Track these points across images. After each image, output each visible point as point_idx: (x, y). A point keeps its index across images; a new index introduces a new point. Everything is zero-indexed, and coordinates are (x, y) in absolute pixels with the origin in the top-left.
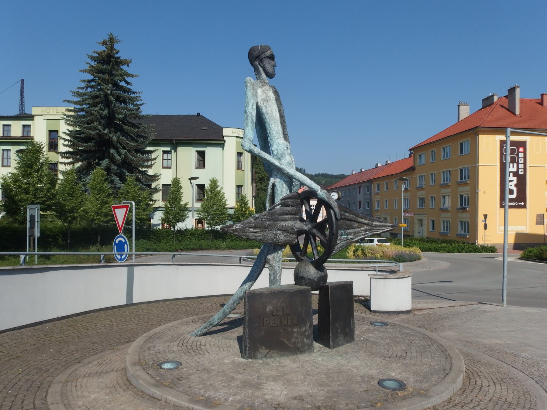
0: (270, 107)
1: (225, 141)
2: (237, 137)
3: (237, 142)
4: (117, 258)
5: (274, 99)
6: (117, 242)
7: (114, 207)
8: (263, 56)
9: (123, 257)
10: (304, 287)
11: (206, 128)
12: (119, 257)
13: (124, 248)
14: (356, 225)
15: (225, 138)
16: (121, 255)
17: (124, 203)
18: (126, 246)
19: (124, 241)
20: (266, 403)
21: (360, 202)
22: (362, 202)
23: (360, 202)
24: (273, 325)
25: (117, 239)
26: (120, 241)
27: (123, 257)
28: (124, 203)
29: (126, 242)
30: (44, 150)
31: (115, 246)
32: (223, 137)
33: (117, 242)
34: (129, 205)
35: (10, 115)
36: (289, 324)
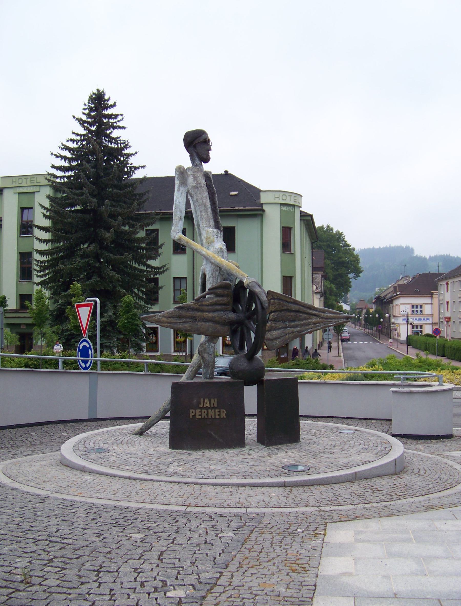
0: (201, 193)
1: (264, 211)
2: (282, 204)
3: (281, 211)
4: (82, 367)
5: (205, 186)
6: (81, 348)
7: (79, 306)
8: (196, 142)
9: (88, 365)
10: (237, 380)
11: (236, 193)
12: (83, 365)
13: (89, 355)
14: (304, 316)
15: (265, 207)
16: (85, 362)
17: (88, 301)
18: (90, 352)
19: (88, 346)
20: (205, 514)
21: (448, 303)
22: (450, 302)
23: (448, 303)
24: (200, 417)
25: (81, 343)
26: (84, 346)
27: (88, 365)
28: (88, 301)
29: (90, 347)
30: (109, 143)
31: (79, 353)
32: (261, 205)
33: (81, 348)
34: (93, 302)
35: (47, 421)
36: (217, 417)
